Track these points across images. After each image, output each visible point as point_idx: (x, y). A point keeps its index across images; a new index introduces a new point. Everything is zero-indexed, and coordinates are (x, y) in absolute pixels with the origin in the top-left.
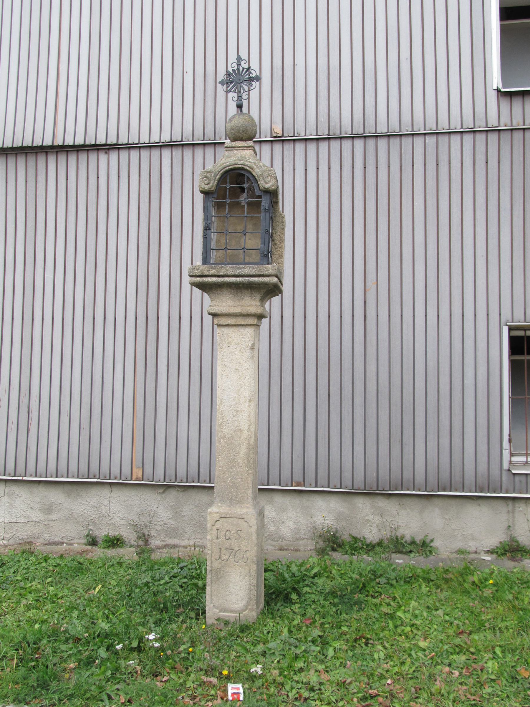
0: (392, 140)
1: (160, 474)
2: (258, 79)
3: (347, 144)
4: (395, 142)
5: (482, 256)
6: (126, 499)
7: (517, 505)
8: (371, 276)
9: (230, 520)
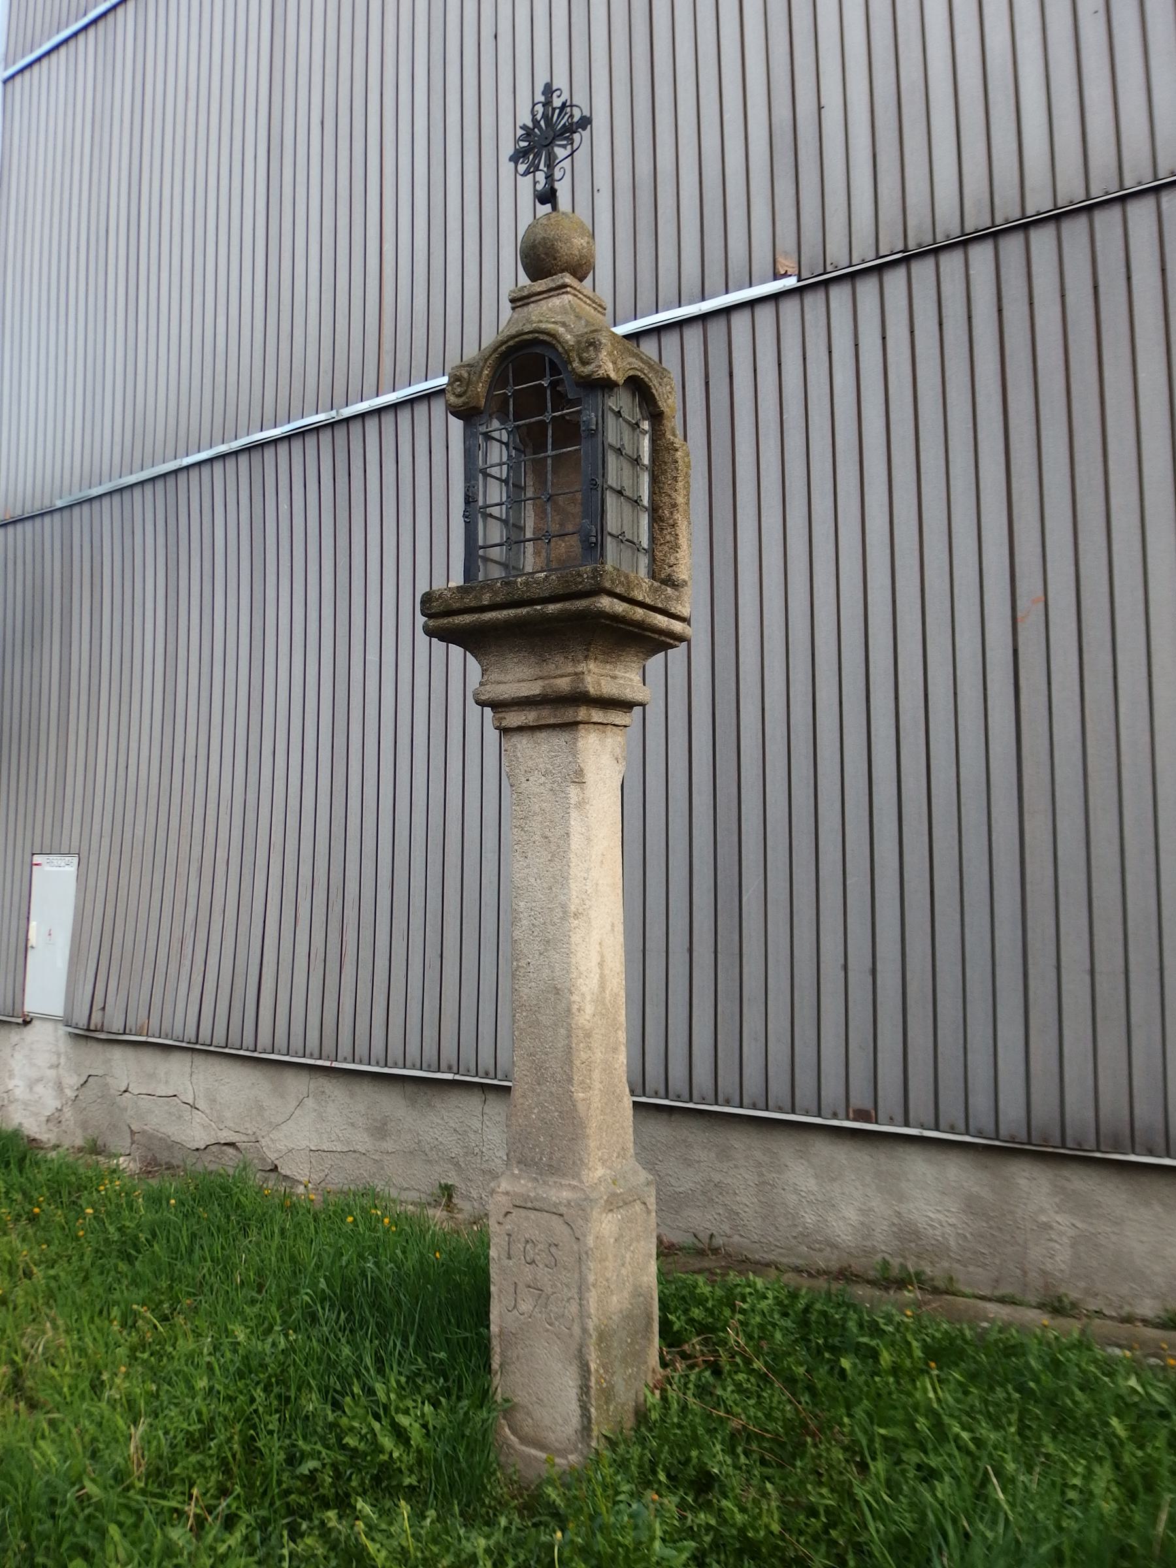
2: (586, 122)
8: (1029, 585)
9: (533, 1215)
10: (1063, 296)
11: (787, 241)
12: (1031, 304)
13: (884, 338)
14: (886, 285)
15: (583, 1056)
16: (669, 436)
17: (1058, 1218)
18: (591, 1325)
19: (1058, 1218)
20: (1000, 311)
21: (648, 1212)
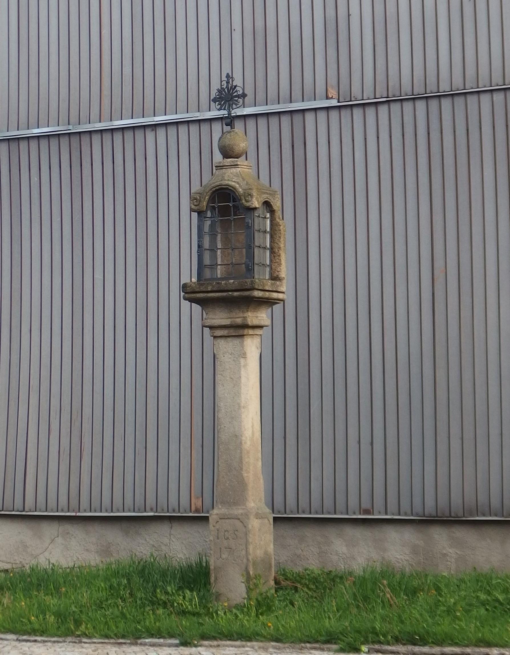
0: (457, 99)
3: (408, 106)
4: (459, 101)
8: (439, 263)
9: (227, 521)
10: (454, 131)
11: (333, 80)
12: (442, 133)
13: (378, 138)
14: (379, 112)
15: (247, 460)
16: (277, 220)
17: (450, 551)
18: (250, 558)
20: (429, 134)
21: (270, 524)
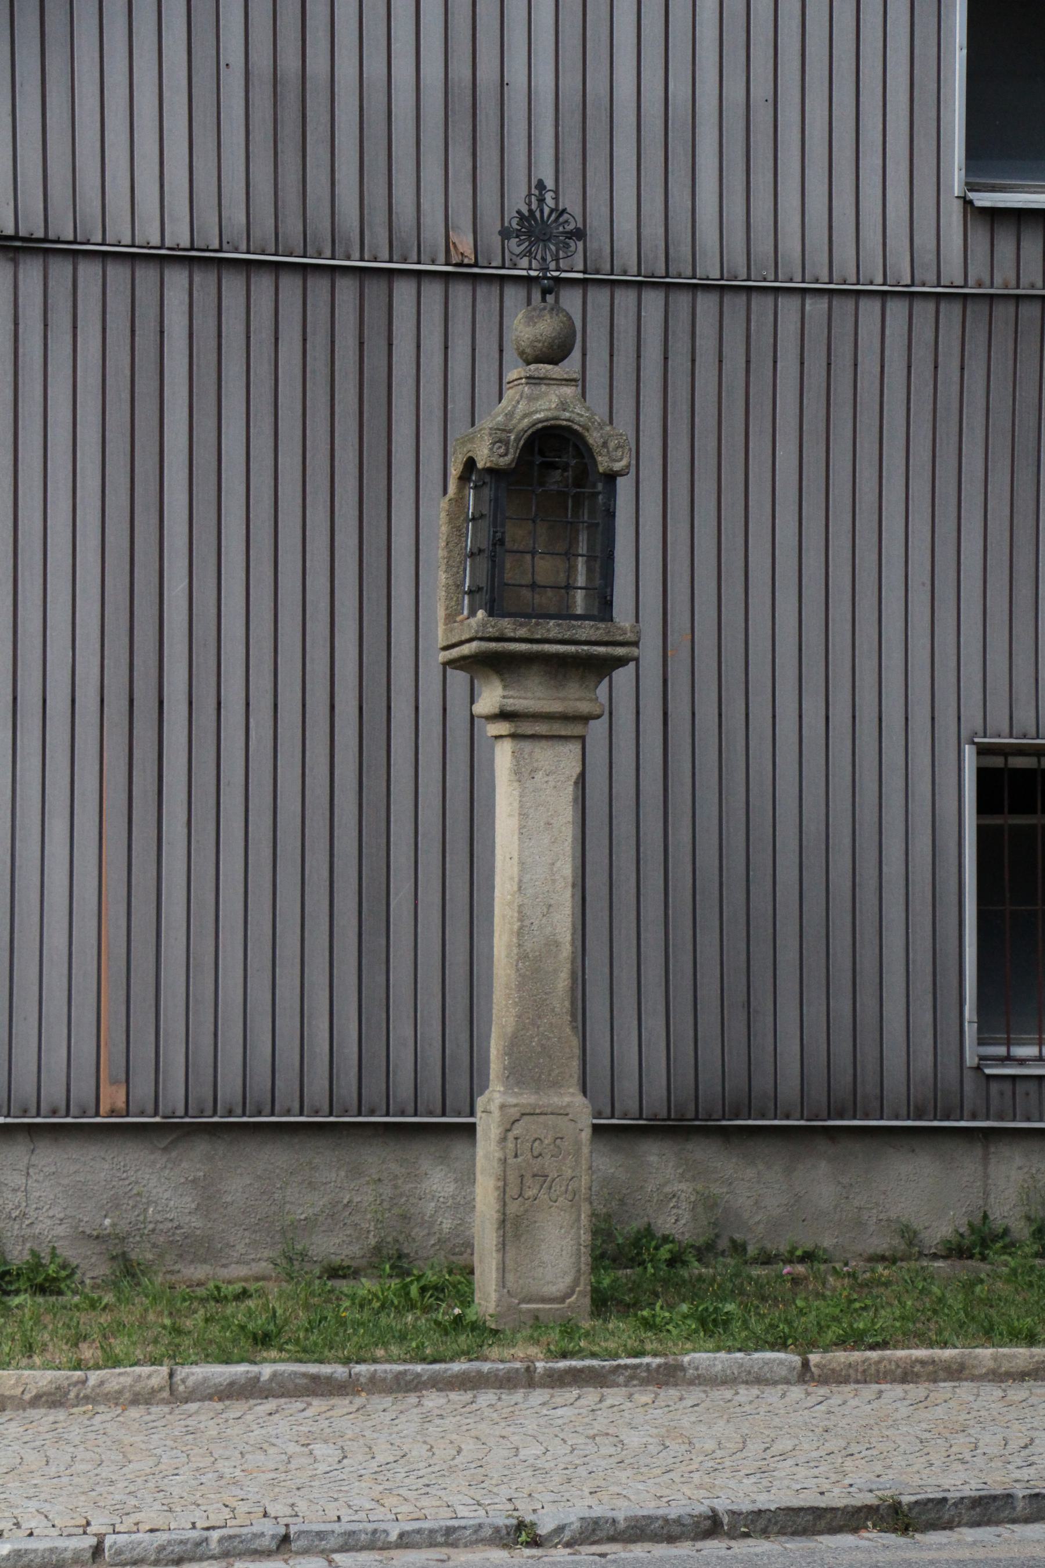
1: (174, 1095)
2: (579, 234)
3: (626, 299)
5: (924, 584)
6: (72, 1169)
7: (992, 1150)
9: (542, 1118)
19: (683, 1186)
